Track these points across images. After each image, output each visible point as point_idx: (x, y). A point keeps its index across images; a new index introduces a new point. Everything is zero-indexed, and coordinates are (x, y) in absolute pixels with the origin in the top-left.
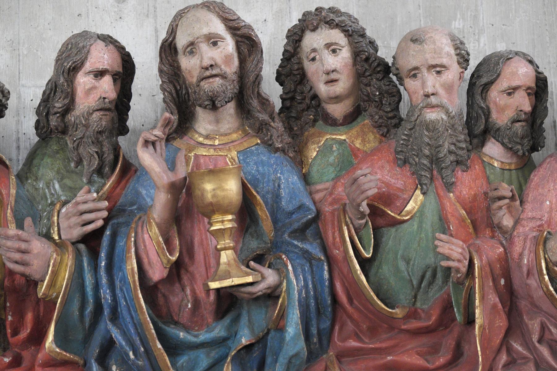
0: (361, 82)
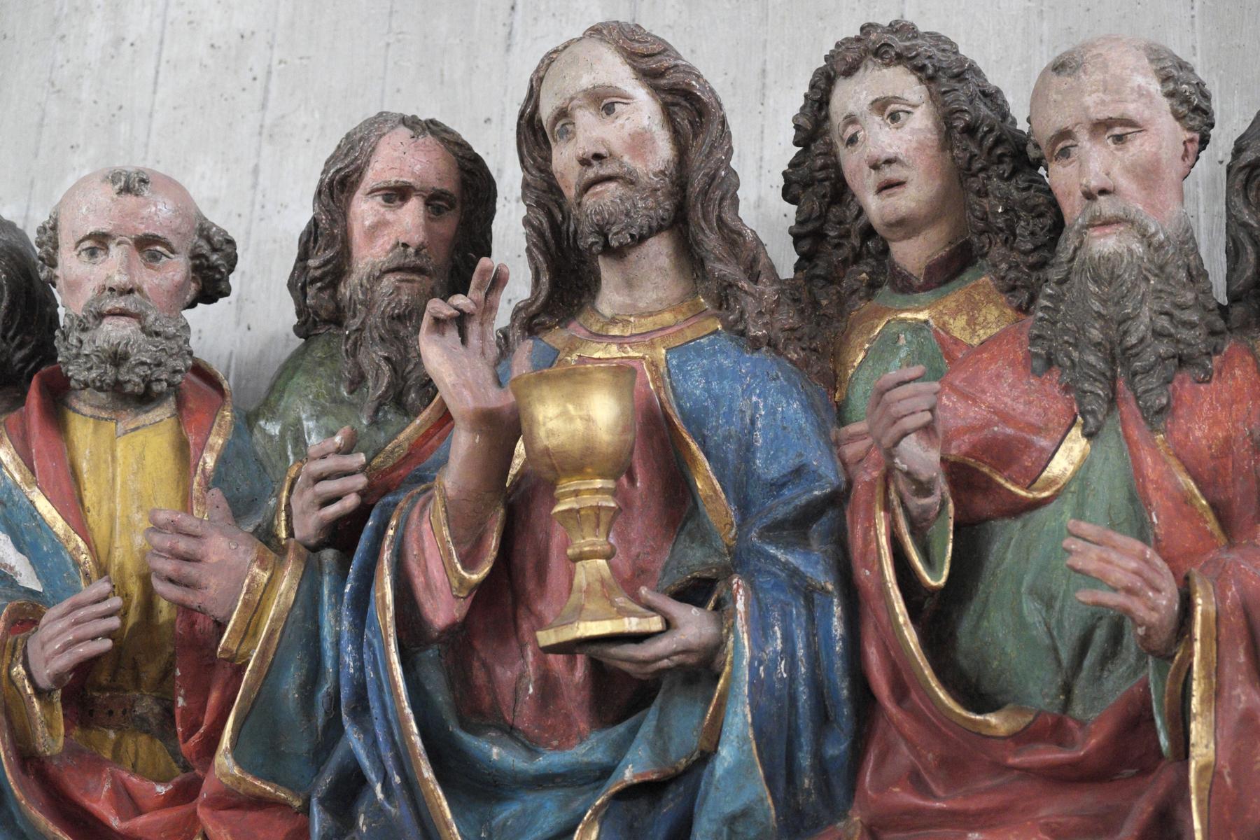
0: (970, 187)
